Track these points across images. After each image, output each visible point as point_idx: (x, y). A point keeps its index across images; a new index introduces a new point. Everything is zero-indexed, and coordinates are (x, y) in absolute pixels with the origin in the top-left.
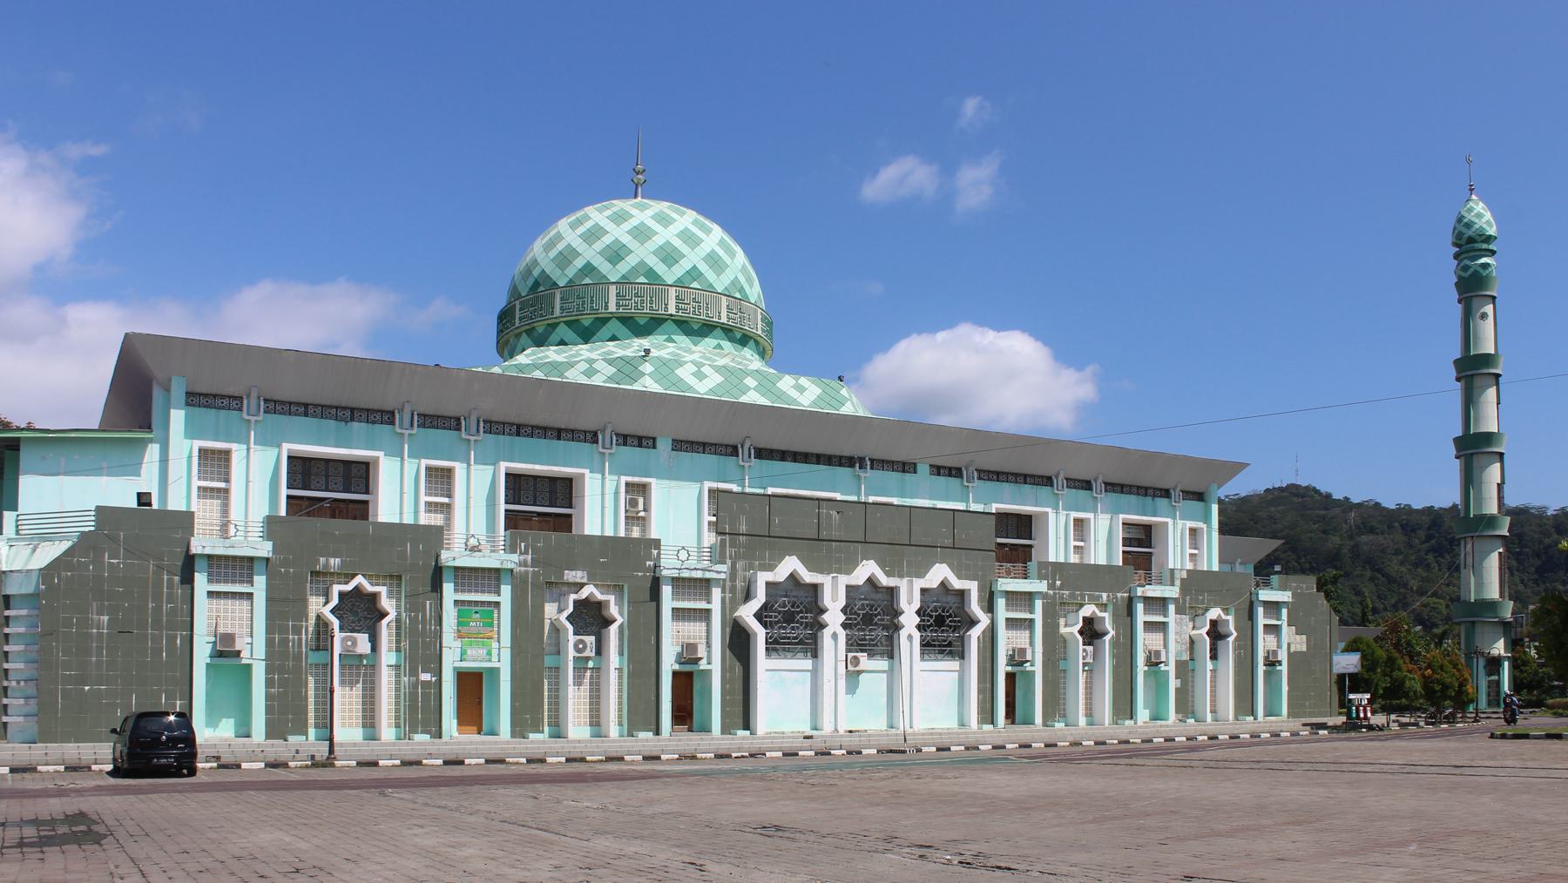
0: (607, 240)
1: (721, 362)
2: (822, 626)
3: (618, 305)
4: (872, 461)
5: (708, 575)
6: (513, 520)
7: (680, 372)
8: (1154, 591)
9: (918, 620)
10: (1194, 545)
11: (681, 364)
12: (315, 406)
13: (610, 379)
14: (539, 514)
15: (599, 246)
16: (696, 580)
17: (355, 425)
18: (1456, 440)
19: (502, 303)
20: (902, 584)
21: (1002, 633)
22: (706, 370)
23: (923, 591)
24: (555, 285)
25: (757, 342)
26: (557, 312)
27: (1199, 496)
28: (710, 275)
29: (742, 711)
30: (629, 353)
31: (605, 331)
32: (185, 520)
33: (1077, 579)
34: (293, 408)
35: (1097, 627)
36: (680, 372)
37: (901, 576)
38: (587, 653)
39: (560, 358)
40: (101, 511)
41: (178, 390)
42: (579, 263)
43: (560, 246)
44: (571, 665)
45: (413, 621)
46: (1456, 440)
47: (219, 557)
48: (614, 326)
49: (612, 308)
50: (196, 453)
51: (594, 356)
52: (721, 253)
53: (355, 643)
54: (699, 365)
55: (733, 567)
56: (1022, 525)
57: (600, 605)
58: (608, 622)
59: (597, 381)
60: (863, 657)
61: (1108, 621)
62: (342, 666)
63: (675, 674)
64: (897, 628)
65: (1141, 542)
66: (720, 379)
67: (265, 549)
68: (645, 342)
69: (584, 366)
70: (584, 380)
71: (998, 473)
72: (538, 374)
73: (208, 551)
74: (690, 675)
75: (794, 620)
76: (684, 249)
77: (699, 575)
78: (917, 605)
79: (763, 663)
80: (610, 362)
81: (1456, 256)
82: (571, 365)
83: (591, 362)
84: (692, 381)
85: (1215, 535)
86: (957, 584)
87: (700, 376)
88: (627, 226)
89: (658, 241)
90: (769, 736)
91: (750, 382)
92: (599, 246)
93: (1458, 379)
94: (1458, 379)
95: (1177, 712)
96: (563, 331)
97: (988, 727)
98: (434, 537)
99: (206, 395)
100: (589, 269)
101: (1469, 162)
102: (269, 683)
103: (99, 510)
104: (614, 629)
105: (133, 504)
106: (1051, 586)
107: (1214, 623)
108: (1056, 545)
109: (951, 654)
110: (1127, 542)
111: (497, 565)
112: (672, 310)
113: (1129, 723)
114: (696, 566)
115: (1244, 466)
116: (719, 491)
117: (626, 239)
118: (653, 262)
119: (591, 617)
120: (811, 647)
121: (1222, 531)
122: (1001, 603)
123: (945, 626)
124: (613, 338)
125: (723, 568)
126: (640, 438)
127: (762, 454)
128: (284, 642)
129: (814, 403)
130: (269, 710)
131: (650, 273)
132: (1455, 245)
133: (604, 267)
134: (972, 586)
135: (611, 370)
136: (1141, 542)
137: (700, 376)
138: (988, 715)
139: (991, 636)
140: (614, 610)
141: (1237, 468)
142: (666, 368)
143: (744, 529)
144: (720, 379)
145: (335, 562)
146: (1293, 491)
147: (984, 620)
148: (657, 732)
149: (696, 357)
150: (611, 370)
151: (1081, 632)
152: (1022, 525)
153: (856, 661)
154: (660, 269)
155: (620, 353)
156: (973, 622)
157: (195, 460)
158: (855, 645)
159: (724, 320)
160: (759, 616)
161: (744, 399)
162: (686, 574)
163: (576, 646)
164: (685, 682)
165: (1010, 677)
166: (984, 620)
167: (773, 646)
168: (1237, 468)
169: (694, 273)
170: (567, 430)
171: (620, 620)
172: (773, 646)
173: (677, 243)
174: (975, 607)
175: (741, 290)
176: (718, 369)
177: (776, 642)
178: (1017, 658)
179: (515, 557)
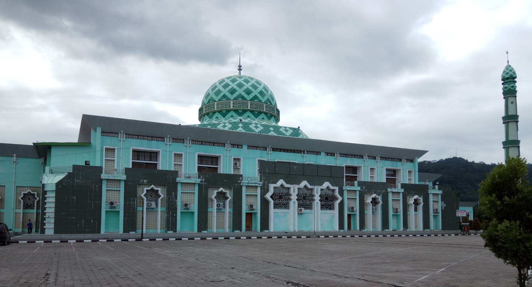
0: (230, 87)
1: (263, 123)
2: (290, 199)
3: (233, 107)
4: (307, 151)
5: (256, 185)
6: (200, 169)
7: (250, 126)
8: (394, 190)
9: (320, 198)
10: (410, 176)
11: (251, 124)
12: (141, 136)
13: (230, 128)
14: (208, 167)
15: (228, 89)
16: (253, 186)
17: (153, 141)
18: (503, 143)
19: (200, 106)
20: (316, 187)
21: (346, 202)
22: (258, 125)
23: (321, 190)
24: (215, 101)
25: (275, 117)
26: (216, 109)
27: (412, 161)
28: (260, 97)
29: (265, 225)
30: (236, 121)
31: (229, 115)
32: (99, 169)
33: (369, 187)
34: (134, 137)
35: (418, 202)
36: (250, 126)
37: (315, 185)
38: (221, 207)
39: (216, 122)
40: (75, 167)
41: (99, 130)
42: (222, 94)
43: (216, 89)
44: (216, 211)
45: (169, 199)
46: (503, 143)
47: (110, 180)
48: (232, 113)
49: (232, 107)
50: (104, 149)
51: (226, 121)
52: (264, 91)
53: (151, 205)
54: (256, 124)
55: (264, 182)
56: (354, 169)
57: (225, 193)
58: (227, 198)
59: (226, 129)
60: (303, 209)
61: (380, 198)
62: (147, 211)
63: (247, 214)
64: (314, 200)
65: (392, 174)
66: (262, 128)
67: (124, 177)
68: (241, 118)
69: (222, 125)
70: (222, 128)
71: (346, 155)
72: (209, 127)
73: (106, 178)
74: (251, 214)
75: (282, 199)
76: (253, 90)
77: (254, 185)
78: (319, 194)
79: (272, 210)
80: (230, 123)
81: (503, 84)
82: (219, 124)
83: (224, 123)
84: (254, 129)
85: (417, 173)
86: (332, 187)
87: (256, 127)
88: (236, 83)
89: (245, 87)
90: (274, 232)
91: (271, 129)
92: (228, 89)
93: (504, 123)
94: (504, 123)
95: (404, 227)
96: (232, 97)
97: (342, 231)
98: (175, 174)
99: (107, 133)
100: (224, 96)
101: (507, 53)
102: (125, 216)
103: (74, 166)
104: (228, 200)
105: (84, 164)
106: (361, 189)
107: (415, 200)
108: (364, 176)
109: (330, 209)
110: (387, 175)
111: (194, 182)
112: (249, 108)
113: (387, 230)
114: (252, 183)
115: (425, 152)
116: (24, 206)
117: (236, 87)
118: (244, 94)
119: (153, 195)
120: (286, 206)
121: (419, 171)
122: (345, 193)
123: (327, 202)
124: (232, 116)
125: (261, 183)
126: (238, 145)
127: (274, 150)
128: (130, 204)
129: (291, 135)
130: (124, 224)
131: (243, 98)
132: (502, 80)
133: (229, 95)
134: (337, 189)
135: (230, 126)
136: (392, 174)
137: (256, 127)
138: (341, 226)
139: (341, 204)
140: (228, 195)
141: (423, 152)
142: (246, 126)
143: (269, 172)
144: (262, 128)
145: (145, 181)
146: (455, 158)
147: (268, 196)
148: (241, 230)
149: (256, 122)
150: (230, 126)
151: (371, 202)
152: (354, 169)
153: (301, 210)
154: (246, 96)
155: (234, 121)
156: (337, 199)
157: (104, 152)
158: (300, 206)
159: (265, 111)
160: (271, 197)
161: (269, 134)
162: (250, 185)
163: (217, 206)
164: (250, 216)
165: (349, 216)
166: (340, 199)
167: (276, 206)
168: (423, 152)
169: (256, 97)
170: (216, 143)
171: (162, 196)
172: (276, 206)
173: (250, 88)
174: (337, 194)
175: (270, 102)
176: (262, 125)
177: (277, 204)
178: (352, 209)
179: (199, 180)
